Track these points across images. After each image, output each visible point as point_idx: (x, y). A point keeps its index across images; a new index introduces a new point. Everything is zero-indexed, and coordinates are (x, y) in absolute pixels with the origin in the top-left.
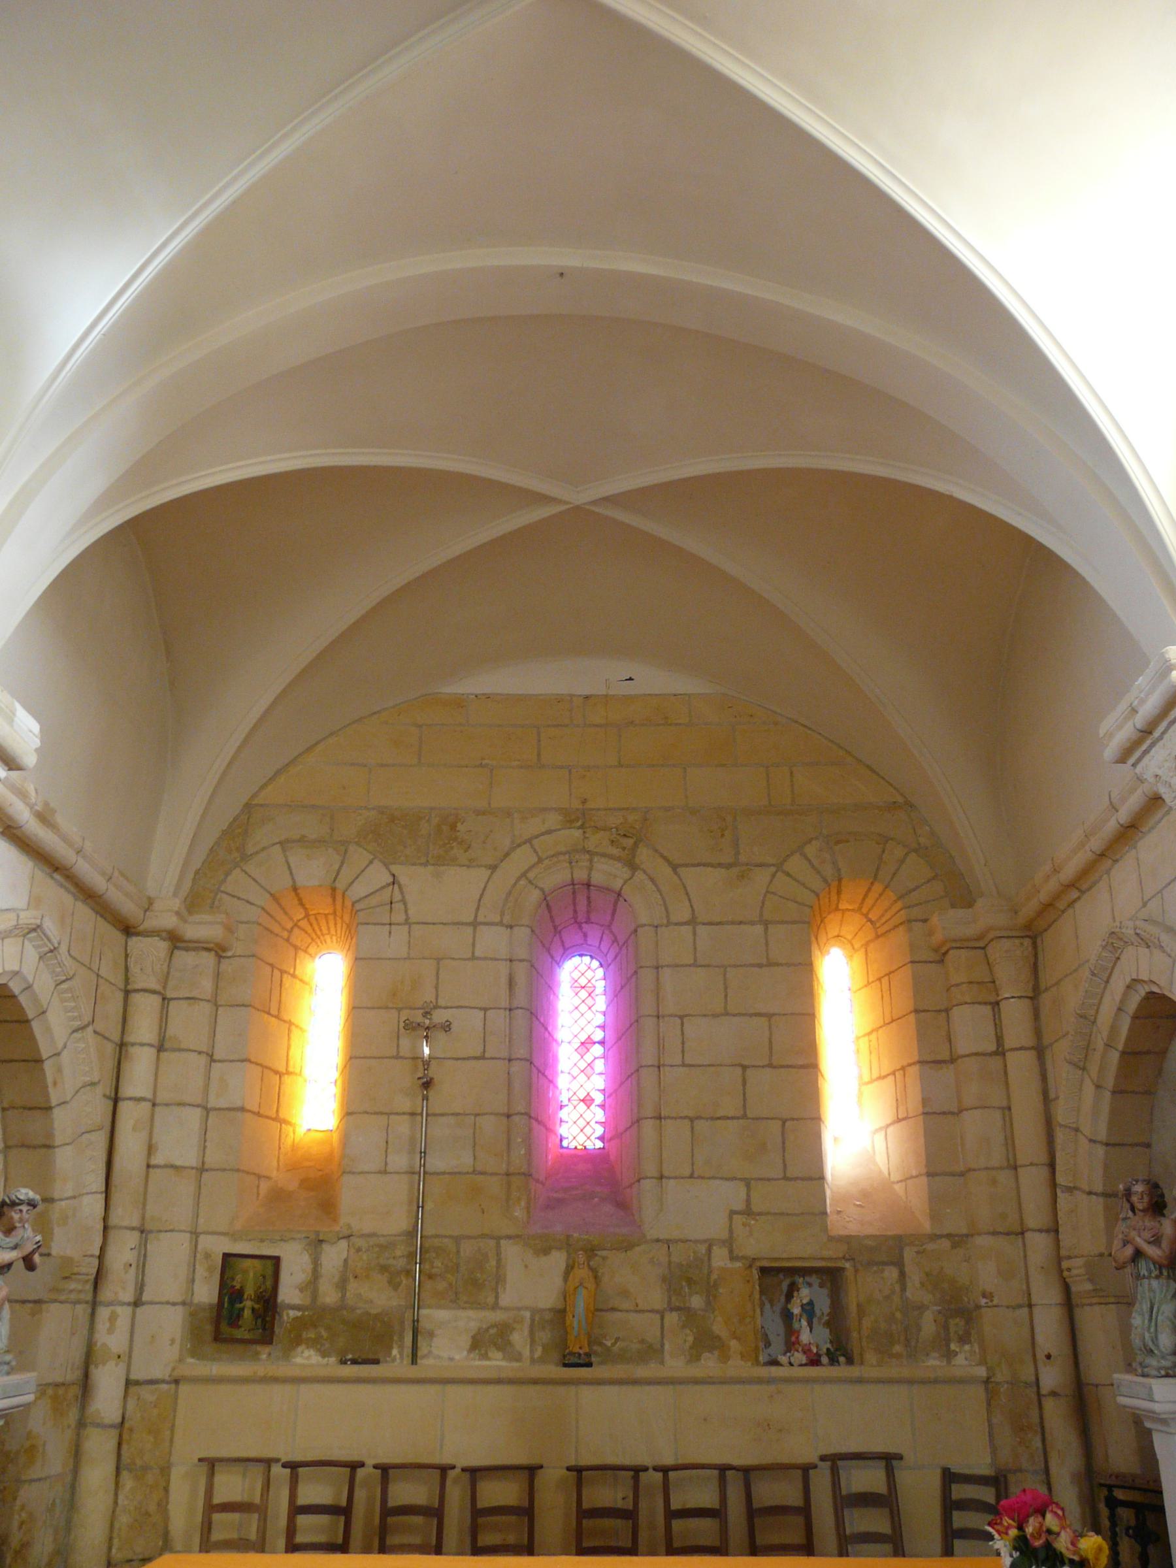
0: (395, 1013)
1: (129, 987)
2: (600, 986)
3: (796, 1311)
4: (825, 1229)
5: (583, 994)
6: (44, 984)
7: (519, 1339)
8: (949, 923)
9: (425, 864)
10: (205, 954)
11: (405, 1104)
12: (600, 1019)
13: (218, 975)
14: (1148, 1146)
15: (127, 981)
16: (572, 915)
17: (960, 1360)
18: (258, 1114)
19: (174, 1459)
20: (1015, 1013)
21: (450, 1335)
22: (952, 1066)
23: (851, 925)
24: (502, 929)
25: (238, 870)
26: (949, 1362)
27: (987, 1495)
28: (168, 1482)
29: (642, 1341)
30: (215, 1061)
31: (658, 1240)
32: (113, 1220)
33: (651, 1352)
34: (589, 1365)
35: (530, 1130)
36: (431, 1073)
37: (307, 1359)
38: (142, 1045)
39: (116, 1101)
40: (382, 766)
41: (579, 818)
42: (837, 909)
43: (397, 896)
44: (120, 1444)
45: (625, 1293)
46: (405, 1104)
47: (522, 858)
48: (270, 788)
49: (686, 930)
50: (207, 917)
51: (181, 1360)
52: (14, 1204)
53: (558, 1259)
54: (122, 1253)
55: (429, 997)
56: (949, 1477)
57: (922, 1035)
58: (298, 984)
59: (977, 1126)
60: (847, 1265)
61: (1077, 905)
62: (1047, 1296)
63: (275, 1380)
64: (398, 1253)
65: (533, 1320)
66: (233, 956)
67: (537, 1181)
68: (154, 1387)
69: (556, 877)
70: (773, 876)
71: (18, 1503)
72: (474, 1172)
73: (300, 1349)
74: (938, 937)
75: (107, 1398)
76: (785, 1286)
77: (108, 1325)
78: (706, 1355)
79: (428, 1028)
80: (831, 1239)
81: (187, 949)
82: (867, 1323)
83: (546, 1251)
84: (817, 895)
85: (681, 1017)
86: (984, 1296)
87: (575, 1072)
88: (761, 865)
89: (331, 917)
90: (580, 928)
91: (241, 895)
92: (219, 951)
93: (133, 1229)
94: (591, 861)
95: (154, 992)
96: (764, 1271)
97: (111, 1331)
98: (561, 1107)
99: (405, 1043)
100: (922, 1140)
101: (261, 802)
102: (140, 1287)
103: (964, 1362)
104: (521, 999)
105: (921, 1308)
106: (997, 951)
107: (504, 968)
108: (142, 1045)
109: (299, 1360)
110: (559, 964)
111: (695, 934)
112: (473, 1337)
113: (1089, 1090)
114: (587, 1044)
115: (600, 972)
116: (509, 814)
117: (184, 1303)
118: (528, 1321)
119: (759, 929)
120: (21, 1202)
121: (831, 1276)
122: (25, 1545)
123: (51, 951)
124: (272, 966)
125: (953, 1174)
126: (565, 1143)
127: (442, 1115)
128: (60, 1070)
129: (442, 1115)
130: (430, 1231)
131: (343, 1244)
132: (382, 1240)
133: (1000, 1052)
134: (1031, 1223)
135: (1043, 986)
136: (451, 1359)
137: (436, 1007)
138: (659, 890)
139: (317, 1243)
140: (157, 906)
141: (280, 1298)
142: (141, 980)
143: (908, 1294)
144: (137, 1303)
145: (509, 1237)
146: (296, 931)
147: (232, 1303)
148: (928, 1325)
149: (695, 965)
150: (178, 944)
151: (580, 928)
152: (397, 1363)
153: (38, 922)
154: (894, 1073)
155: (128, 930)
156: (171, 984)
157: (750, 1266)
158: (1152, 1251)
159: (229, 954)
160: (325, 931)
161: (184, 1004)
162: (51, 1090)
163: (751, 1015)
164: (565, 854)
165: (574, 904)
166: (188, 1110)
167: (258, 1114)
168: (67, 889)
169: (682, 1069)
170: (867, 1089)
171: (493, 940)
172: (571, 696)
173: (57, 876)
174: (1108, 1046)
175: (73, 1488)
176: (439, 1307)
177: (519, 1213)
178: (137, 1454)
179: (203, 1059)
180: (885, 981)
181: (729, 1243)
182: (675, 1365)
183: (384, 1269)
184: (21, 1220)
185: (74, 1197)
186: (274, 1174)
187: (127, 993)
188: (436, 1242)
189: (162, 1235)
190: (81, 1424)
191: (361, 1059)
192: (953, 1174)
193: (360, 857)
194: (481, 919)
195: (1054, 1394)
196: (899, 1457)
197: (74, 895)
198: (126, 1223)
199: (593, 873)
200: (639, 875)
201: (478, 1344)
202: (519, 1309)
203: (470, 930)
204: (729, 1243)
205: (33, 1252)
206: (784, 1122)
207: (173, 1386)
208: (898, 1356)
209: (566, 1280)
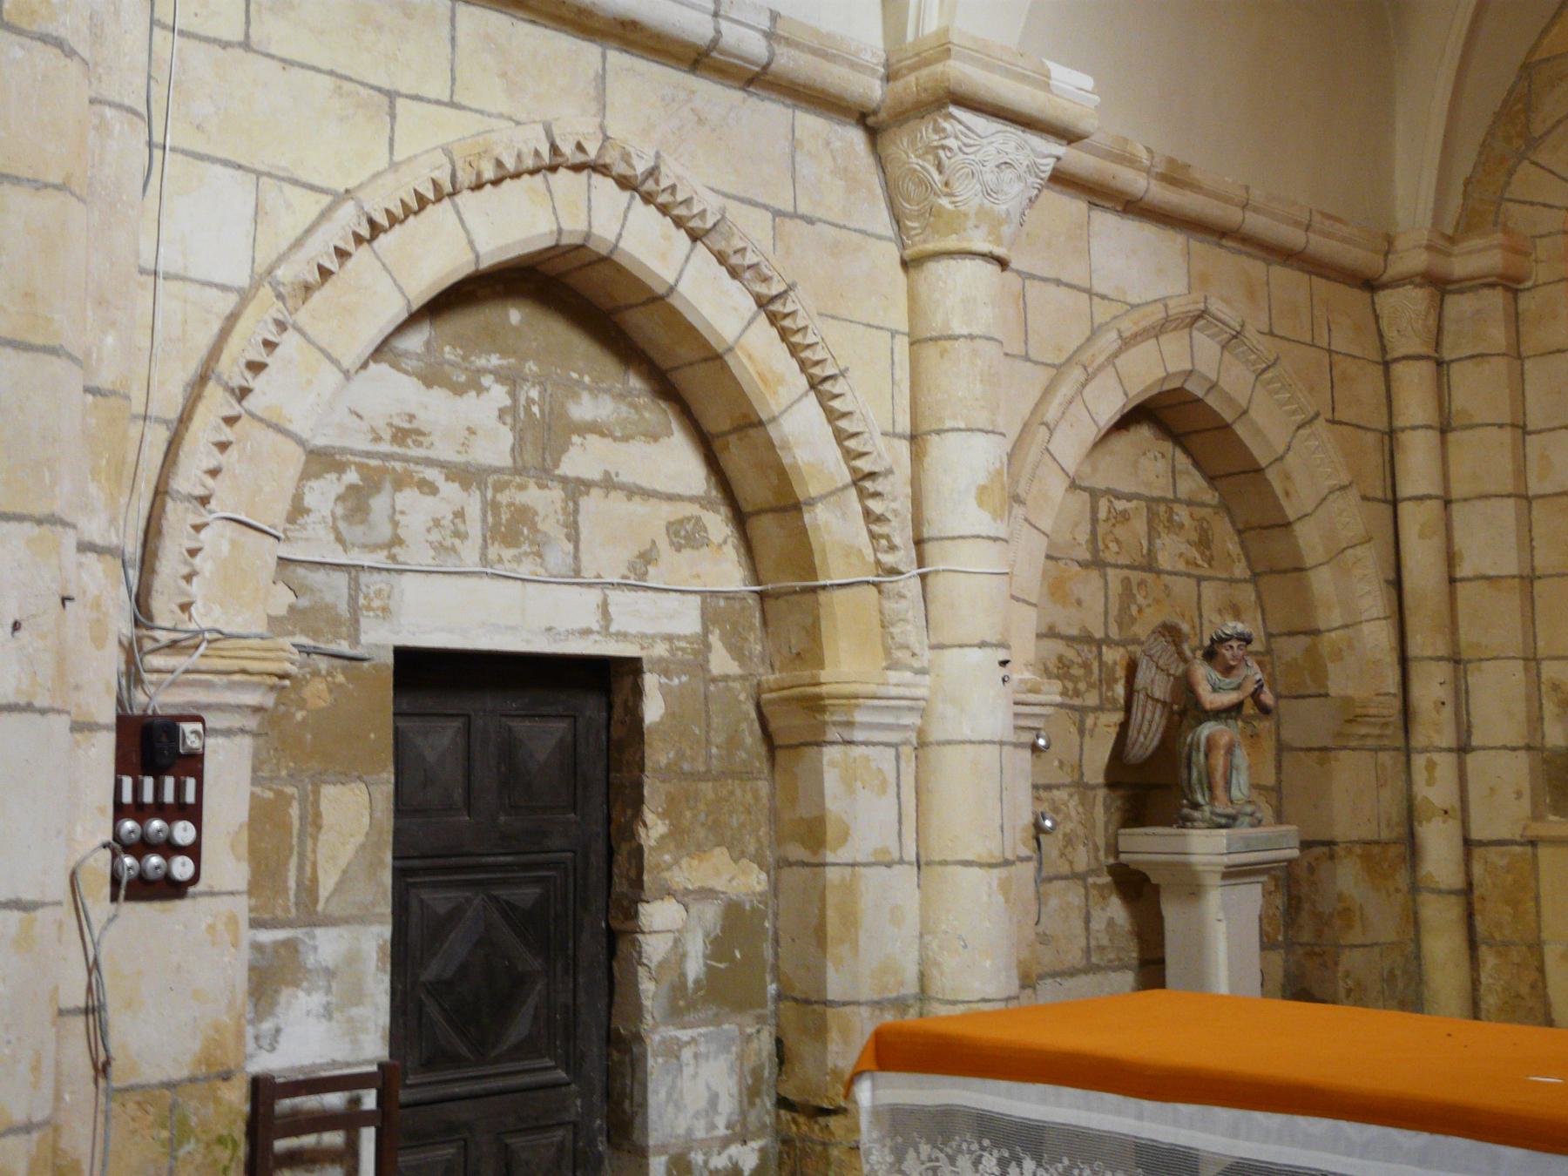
1: (1389, 357)
10: (1486, 292)
15: (1384, 349)
19: (1545, 935)
25: (1526, 163)
28: (1542, 961)
30: (1530, 433)
38: (1414, 428)
39: (1394, 503)
48: (1556, 30)
54: (1430, 688)
66: (1535, 286)
68: (1504, 849)
71: (1341, 968)
75: (1440, 854)
77: (1425, 774)
81: (1461, 292)
91: (1535, 200)
92: (1510, 284)
93: (1440, 659)
95: (1428, 358)
97: (1431, 782)
101: (1545, 55)
108: (1414, 428)
120: (1230, 638)
123: (1235, 337)
140: (1400, 244)
150: (1449, 287)
153: (1201, 306)
155: (1370, 285)
156: (1447, 342)
161: (1469, 364)
162: (1284, 502)
168: (1249, 255)
173: (1224, 242)
185: (1346, 626)
189: (1485, 664)
197: (1264, 260)
198: (1429, 653)
207: (1529, 849)
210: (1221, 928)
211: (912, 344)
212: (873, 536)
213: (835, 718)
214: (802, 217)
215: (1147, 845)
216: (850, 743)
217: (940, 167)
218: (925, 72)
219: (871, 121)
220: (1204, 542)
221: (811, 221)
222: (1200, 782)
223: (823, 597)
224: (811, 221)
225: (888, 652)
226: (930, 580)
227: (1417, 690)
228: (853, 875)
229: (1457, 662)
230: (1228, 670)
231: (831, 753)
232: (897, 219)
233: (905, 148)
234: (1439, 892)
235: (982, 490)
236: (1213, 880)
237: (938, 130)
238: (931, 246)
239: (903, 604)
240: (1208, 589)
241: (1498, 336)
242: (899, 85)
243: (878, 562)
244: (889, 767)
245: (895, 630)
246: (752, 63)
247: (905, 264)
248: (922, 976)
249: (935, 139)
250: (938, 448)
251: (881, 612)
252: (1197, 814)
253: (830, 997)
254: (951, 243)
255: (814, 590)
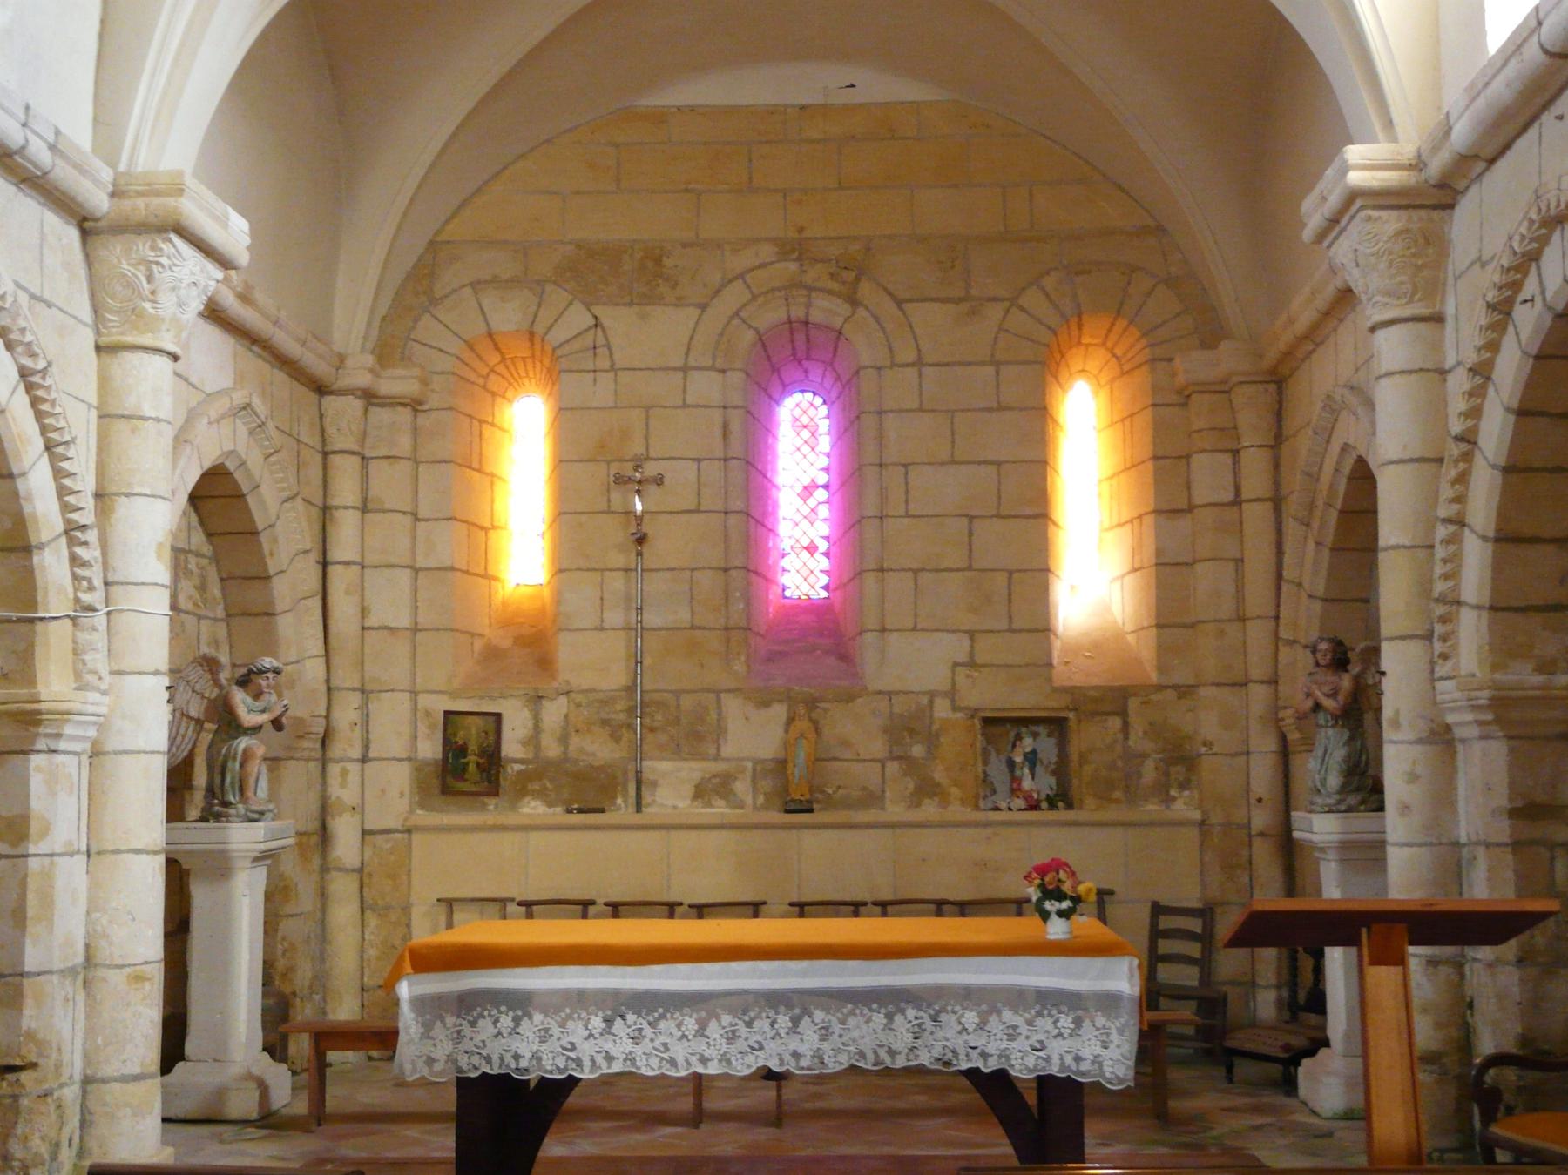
0: (604, 465)
1: (328, 448)
2: (824, 425)
3: (1018, 759)
4: (1049, 680)
5: (806, 434)
6: (254, 459)
7: (742, 787)
8: (1193, 365)
9: (631, 304)
10: (400, 409)
11: (618, 560)
12: (824, 462)
13: (415, 431)
14: (1367, 601)
15: (324, 441)
16: (786, 355)
17: (1179, 805)
18: (467, 572)
19: (413, 899)
20: (1255, 465)
21: (673, 785)
22: (1189, 516)
23: (1097, 359)
24: (714, 374)
26: (1168, 807)
27: (1195, 925)
29: (864, 789)
31: (880, 692)
32: (333, 684)
33: (872, 799)
34: (811, 811)
35: (749, 584)
36: (645, 528)
37: (533, 808)
38: (347, 508)
40: (578, 193)
41: (796, 249)
42: (1079, 343)
43: (601, 340)
44: (361, 887)
45: (845, 744)
46: (618, 560)
47: (735, 295)
49: (911, 373)
50: (400, 372)
51: (411, 812)
52: (261, 672)
53: (779, 711)
55: (639, 449)
56: (1158, 910)
57: (1160, 481)
58: (497, 431)
59: (1209, 580)
60: (1071, 715)
61: (1314, 356)
62: (1264, 746)
63: (504, 828)
64: (619, 708)
65: (754, 770)
67: (757, 634)
69: (771, 315)
70: (1007, 311)
71: (280, 934)
72: (692, 627)
73: (526, 799)
74: (1181, 379)
75: (346, 845)
76: (1012, 735)
78: (927, 801)
79: (639, 482)
80: (1055, 690)
82: (1088, 769)
83: (765, 704)
84: (1055, 333)
85: (905, 466)
86: (1205, 744)
87: (798, 518)
88: (995, 299)
89: (529, 361)
90: (800, 362)
92: (415, 405)
93: (354, 689)
94: (809, 296)
95: (353, 453)
96: (987, 721)
97: (343, 785)
98: (784, 555)
99: (616, 497)
100: (1153, 590)
102: (366, 746)
103: (1183, 807)
104: (736, 448)
105: (1144, 756)
106: (1241, 396)
107: (717, 416)
108: (347, 508)
109: (526, 810)
110: (778, 403)
111: (920, 375)
112: (696, 787)
113: (1311, 545)
114: (809, 490)
115: (824, 410)
116: (719, 246)
117: (409, 759)
118: (749, 773)
119: (990, 370)
120: (268, 670)
121: (1057, 725)
122: (291, 969)
124: (470, 417)
125: (1185, 626)
126: (788, 593)
127: (657, 570)
128: (275, 540)
129: (657, 570)
130: (648, 687)
131: (563, 700)
132: (601, 696)
133: (1237, 502)
134: (1255, 673)
135: (1285, 433)
136: (675, 807)
137: (648, 458)
138: (882, 328)
139: (536, 700)
140: (349, 363)
141: (503, 754)
142: (339, 441)
143: (1131, 743)
144: (364, 760)
145: (729, 691)
146: (493, 377)
147: (456, 757)
148: (1149, 772)
149: (921, 410)
151: (800, 362)
152: (622, 810)
154: (1131, 521)
156: (369, 442)
157: (972, 717)
158: (1329, 703)
159: (426, 407)
160: (523, 374)
161: (384, 463)
162: (268, 560)
163: (979, 463)
164: (779, 289)
165: (792, 341)
166: (398, 571)
167: (467, 572)
169: (906, 520)
170: (1111, 535)
171: (705, 386)
172: (786, 106)
173: (255, 348)
174: (1328, 505)
175: (323, 923)
176: (663, 759)
177: (739, 667)
178: (380, 892)
179: (408, 519)
180: (1127, 422)
181: (952, 694)
182: (895, 811)
183: (605, 723)
184: (268, 686)
186: (487, 632)
187: (325, 454)
188: (656, 696)
190: (325, 869)
191: (570, 515)
192: (1185, 626)
193: (557, 296)
194: (692, 362)
195: (1261, 834)
196: (1111, 893)
199: (811, 311)
200: (861, 312)
201: (701, 793)
202: (743, 759)
203: (681, 374)
204: (952, 694)
205: (281, 715)
206: (1011, 573)
207: (406, 836)
208: (1117, 801)
209: (786, 731)
210: (246, 901)
211: (100, 417)
212: (75, 577)
213: (49, 731)
214: (44, 301)
215: (198, 836)
216: (55, 751)
217: (150, 278)
218: (156, 201)
219: (87, 225)
220: (202, 588)
221: (49, 305)
222: (232, 783)
223: (39, 626)
224: (49, 305)
225: (78, 675)
226: (113, 616)
227: (336, 714)
228: (52, 863)
229: (363, 692)
230: (257, 696)
231: (36, 760)
232: (96, 310)
233: (118, 256)
234: (347, 871)
235: (160, 545)
236: (239, 863)
237: (154, 248)
238: (129, 339)
239: (95, 636)
240: (205, 625)
241: (404, 443)
242: (126, 204)
243: (77, 600)
244: (74, 772)
245: (87, 657)
246: (36, 166)
247: (98, 348)
248: (87, 946)
249: (151, 255)
250: (124, 509)
251: (75, 642)
252: (232, 811)
253: (27, 969)
254: (147, 340)
255: (32, 621)
